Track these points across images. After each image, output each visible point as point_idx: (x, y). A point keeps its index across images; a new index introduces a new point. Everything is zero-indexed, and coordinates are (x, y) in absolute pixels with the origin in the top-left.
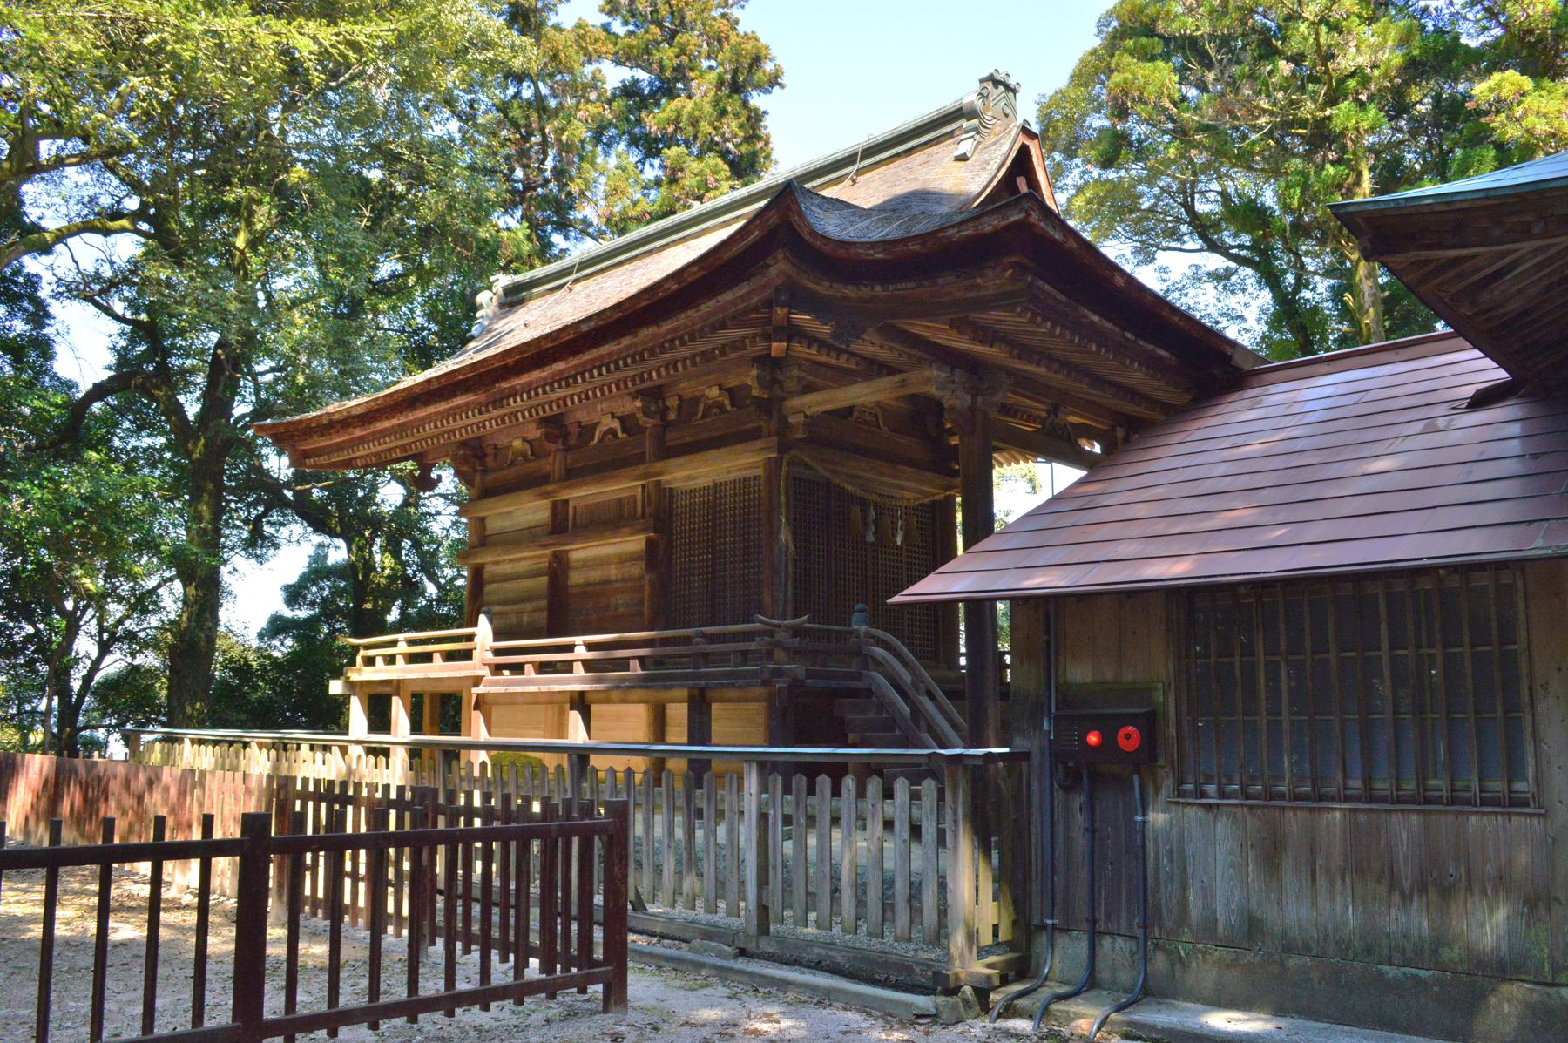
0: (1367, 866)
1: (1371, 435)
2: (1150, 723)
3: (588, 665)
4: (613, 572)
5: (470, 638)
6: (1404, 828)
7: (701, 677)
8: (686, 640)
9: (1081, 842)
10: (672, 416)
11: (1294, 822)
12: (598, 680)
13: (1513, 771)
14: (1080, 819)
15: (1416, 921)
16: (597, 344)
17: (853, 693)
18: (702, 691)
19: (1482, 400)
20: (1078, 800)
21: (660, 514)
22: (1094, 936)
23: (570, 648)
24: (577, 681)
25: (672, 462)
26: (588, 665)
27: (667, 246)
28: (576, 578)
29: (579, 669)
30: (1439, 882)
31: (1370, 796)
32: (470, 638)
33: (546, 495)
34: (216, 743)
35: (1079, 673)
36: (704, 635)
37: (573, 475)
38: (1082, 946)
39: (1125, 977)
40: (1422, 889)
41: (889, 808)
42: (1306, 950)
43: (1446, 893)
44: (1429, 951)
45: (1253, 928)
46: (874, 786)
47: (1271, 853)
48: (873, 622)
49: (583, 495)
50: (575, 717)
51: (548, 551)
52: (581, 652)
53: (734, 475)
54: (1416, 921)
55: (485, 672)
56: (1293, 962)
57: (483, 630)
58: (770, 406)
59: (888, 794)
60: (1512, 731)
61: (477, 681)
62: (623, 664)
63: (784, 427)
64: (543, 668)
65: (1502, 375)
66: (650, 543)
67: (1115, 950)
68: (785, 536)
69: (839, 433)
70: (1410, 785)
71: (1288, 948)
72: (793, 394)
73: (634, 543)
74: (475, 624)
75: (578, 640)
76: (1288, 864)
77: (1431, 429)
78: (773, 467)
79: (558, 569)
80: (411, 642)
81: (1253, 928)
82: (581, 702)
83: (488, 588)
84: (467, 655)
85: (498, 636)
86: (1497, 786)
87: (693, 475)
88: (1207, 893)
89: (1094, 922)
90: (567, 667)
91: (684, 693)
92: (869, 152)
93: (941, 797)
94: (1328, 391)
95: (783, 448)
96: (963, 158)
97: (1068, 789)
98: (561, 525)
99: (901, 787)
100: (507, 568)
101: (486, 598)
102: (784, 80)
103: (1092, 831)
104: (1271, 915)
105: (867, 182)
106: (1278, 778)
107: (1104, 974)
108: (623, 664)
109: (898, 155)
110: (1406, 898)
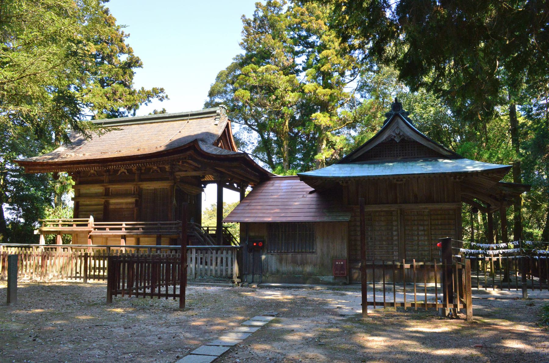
0: (294, 262)
1: (294, 196)
2: (263, 242)
3: (126, 229)
4: (124, 206)
5: (87, 221)
6: (299, 256)
7: (160, 232)
8: (156, 224)
9: (252, 260)
10: (143, 171)
11: (284, 256)
12: (128, 232)
13: (313, 249)
14: (251, 257)
15: (299, 269)
16: (459, 280)
17: (191, 236)
18: (160, 235)
19: (311, 193)
20: (252, 254)
21: (139, 194)
22: (253, 275)
23: (121, 225)
24: (123, 232)
25: (144, 183)
26: (126, 229)
27: (133, 124)
28: (112, 207)
29: (124, 230)
30: (303, 263)
31: (295, 252)
32: (87, 221)
33: (103, 186)
34: (15, 247)
35: (252, 234)
36: (160, 223)
37: (111, 182)
38: (251, 276)
39: (258, 280)
40: (301, 264)
41: (222, 256)
42: (285, 274)
43: (304, 265)
44: (301, 273)
45: (278, 271)
46: (219, 252)
47: (281, 261)
48: (195, 222)
49: (114, 187)
50: (123, 240)
51: (104, 200)
52: (124, 226)
53: (161, 187)
54: (299, 269)
55: (92, 229)
56: (283, 276)
57: (91, 219)
58: (172, 173)
59: (222, 253)
60: (313, 244)
61: (90, 232)
62: (138, 229)
63: (175, 179)
64: (111, 229)
65: (313, 189)
66: (136, 201)
67: (257, 276)
68: (174, 202)
69: (184, 180)
70: (300, 250)
71: (283, 274)
72: (177, 172)
73: (131, 200)
74: (89, 218)
75: (124, 223)
76: (283, 263)
77: (303, 197)
78: (172, 187)
79: (106, 205)
80: (126, 225)
81: (278, 271)
82: (124, 237)
83: (80, 207)
84: (86, 225)
85: (95, 220)
86: (311, 250)
87: (149, 186)
88: (271, 267)
89: (253, 272)
90: (120, 229)
91: (156, 236)
92: (192, 115)
93: (232, 253)
94: (286, 185)
95: (175, 183)
96: (217, 125)
97: (249, 252)
98: (107, 194)
99: (225, 252)
100: (85, 203)
101: (80, 210)
102: (143, 66)
103: (253, 258)
104: (281, 269)
105: (192, 123)
106: (282, 250)
107: (255, 280)
108: (138, 229)
109: (199, 118)
110: (299, 266)
